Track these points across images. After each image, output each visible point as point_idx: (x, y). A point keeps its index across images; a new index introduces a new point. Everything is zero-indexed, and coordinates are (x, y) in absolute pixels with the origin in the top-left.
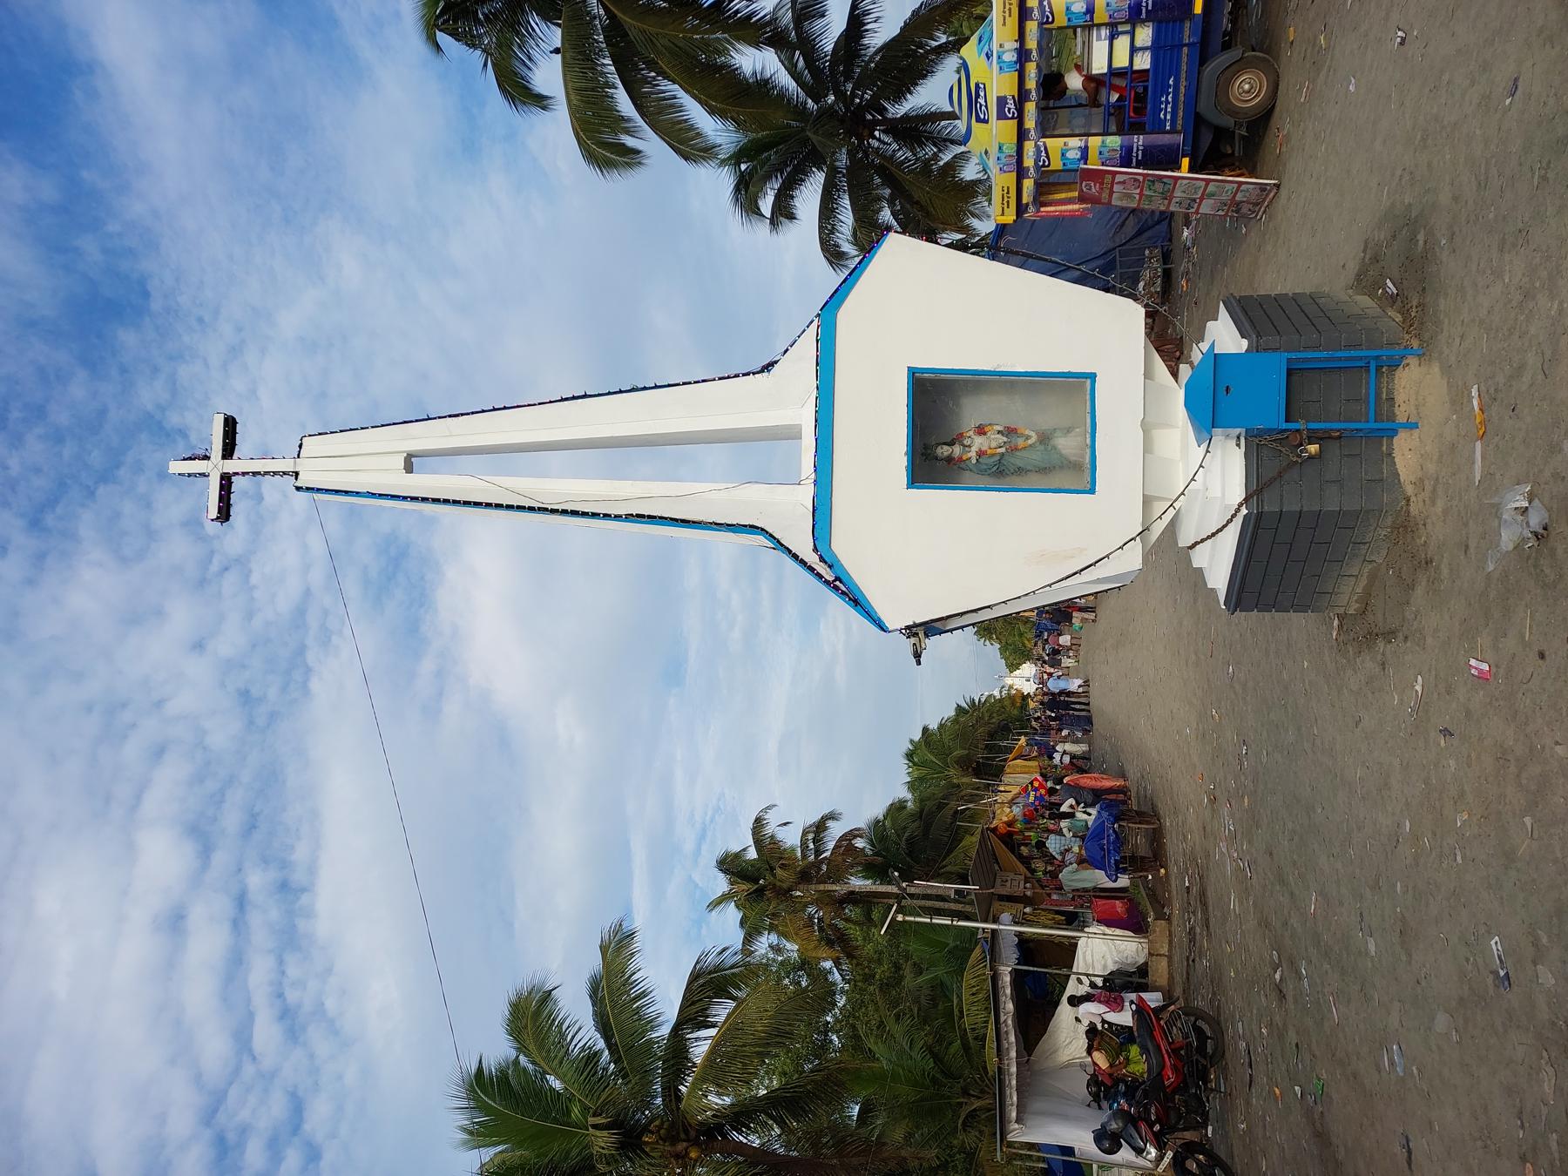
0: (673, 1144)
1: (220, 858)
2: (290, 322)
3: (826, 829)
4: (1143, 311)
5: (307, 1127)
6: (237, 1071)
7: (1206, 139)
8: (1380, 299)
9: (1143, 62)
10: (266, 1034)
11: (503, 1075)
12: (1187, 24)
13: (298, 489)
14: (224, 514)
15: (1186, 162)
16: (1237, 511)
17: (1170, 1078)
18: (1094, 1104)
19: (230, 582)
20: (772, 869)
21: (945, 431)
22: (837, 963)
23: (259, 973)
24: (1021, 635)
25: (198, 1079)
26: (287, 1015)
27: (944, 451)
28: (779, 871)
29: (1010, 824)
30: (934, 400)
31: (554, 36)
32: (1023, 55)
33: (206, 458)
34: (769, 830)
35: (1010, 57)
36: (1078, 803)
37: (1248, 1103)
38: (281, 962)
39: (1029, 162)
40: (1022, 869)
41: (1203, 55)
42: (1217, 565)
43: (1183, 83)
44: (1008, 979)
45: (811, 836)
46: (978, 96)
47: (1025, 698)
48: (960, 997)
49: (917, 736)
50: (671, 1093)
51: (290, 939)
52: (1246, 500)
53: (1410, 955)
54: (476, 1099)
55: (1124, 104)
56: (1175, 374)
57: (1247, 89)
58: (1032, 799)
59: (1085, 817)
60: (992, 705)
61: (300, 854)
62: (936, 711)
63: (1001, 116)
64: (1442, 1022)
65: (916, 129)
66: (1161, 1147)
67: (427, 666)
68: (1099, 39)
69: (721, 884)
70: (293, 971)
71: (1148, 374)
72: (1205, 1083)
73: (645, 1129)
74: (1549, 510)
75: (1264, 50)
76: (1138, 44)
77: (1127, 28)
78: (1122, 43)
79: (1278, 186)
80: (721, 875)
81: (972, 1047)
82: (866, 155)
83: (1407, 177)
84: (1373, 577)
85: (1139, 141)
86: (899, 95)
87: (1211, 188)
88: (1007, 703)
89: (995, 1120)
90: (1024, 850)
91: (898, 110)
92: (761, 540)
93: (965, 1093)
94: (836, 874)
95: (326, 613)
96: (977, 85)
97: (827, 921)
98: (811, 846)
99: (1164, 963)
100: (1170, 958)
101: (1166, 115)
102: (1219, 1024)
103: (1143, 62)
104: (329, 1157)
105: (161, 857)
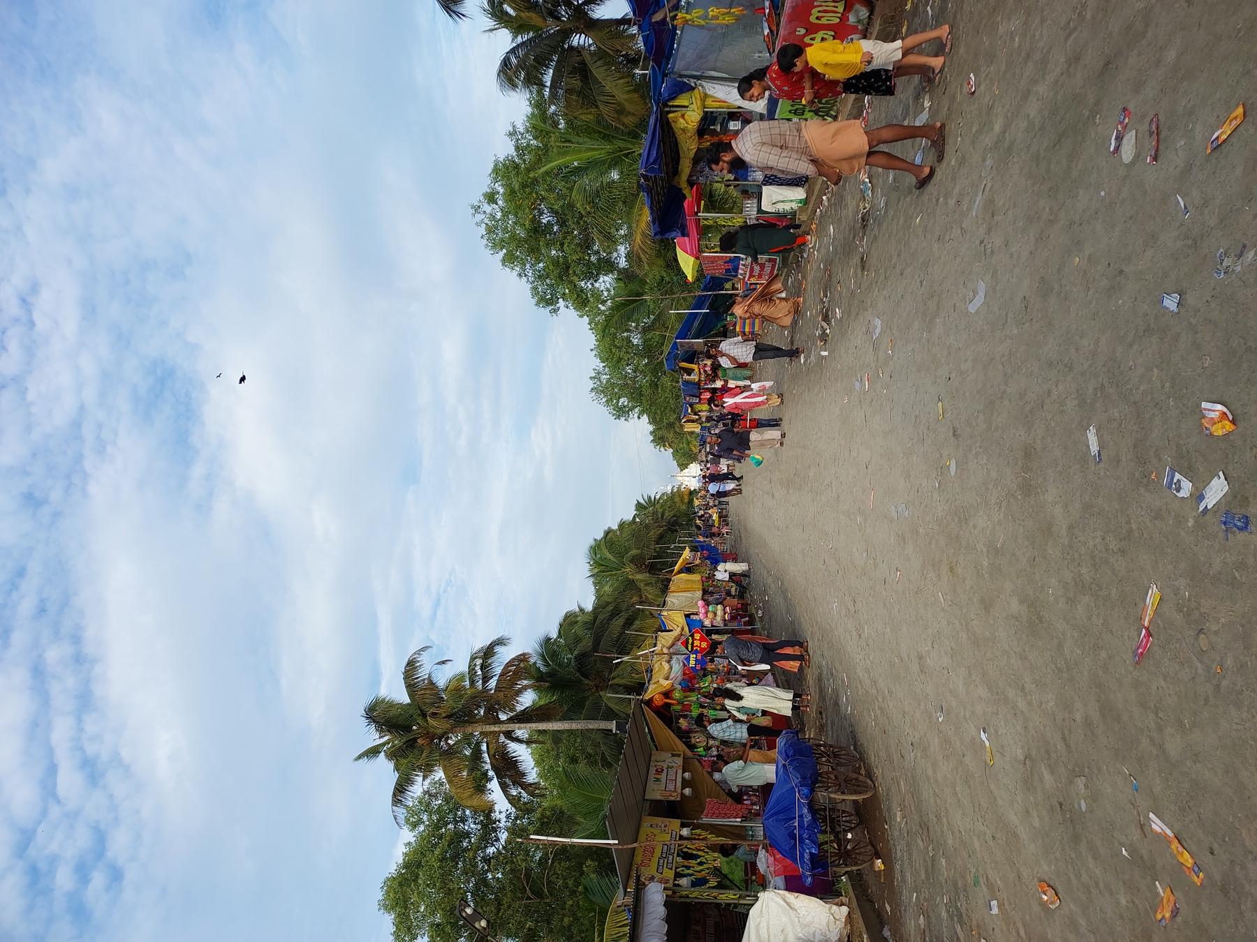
3: (493, 654)
5: (110, 854)
6: (45, 812)
10: (69, 781)
23: (61, 731)
24: (688, 443)
29: (667, 694)
34: (423, 673)
40: (681, 747)
45: (479, 662)
47: (692, 493)
49: (600, 536)
51: (85, 701)
60: (666, 501)
62: (619, 510)
67: (198, 470)
69: (373, 737)
70: (90, 728)
88: (677, 499)
90: (683, 723)
98: (479, 672)
104: (131, 874)
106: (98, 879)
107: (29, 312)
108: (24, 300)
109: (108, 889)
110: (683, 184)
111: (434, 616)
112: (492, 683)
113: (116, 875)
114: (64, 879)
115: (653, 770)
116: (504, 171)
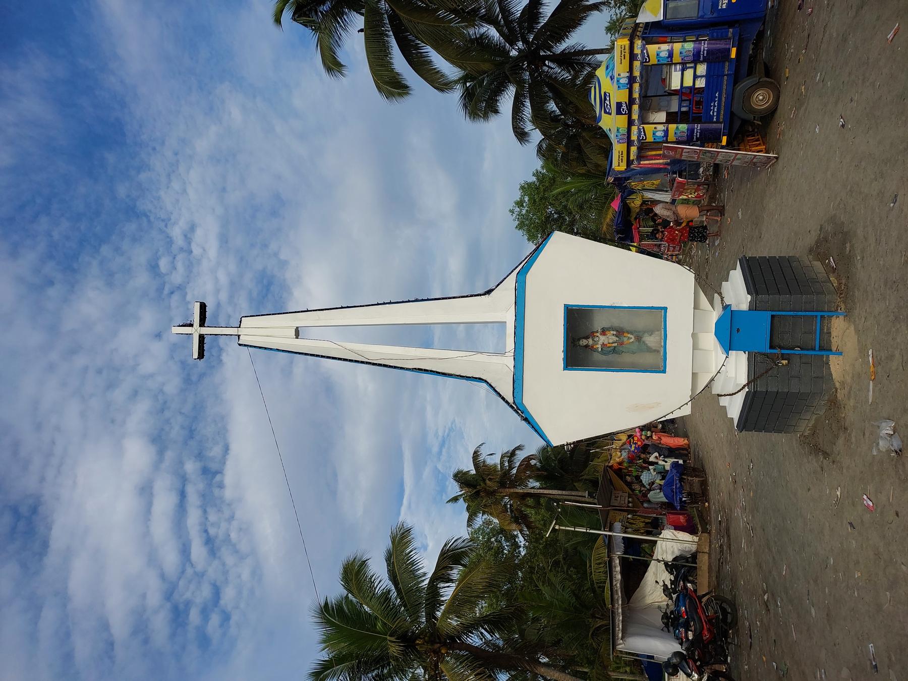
0: (432, 645)
1: (169, 455)
2: (202, 146)
4: (691, 276)
5: (222, 602)
6: (183, 572)
7: (737, 124)
8: (827, 266)
9: (701, 83)
10: (198, 551)
11: (339, 607)
12: (727, 64)
13: (240, 345)
14: (201, 355)
15: (725, 139)
16: (743, 388)
17: (706, 636)
18: (666, 629)
19: (175, 298)
20: (484, 480)
21: (585, 339)
22: (521, 531)
23: (193, 517)
25: (163, 577)
26: (209, 541)
27: (584, 342)
28: (487, 482)
29: (620, 463)
30: (578, 321)
31: (358, 21)
32: (632, 79)
33: (191, 325)
35: (624, 81)
36: (660, 456)
37: (749, 656)
38: (205, 512)
39: (634, 137)
40: (627, 489)
41: (736, 79)
42: (734, 408)
43: (724, 96)
44: (617, 561)
46: (605, 99)
48: (590, 566)
50: (431, 616)
52: (748, 384)
53: (831, 628)
54: (324, 618)
55: (692, 107)
56: (712, 303)
57: (761, 99)
58: (633, 449)
59: (664, 463)
61: (216, 451)
63: (619, 112)
64: (845, 673)
65: (571, 59)
66: (701, 674)
68: (675, 70)
69: (454, 489)
70: (212, 517)
71: (696, 307)
72: (726, 639)
73: (418, 637)
74: (903, 442)
75: (770, 75)
76: (698, 73)
77: (692, 65)
78: (689, 73)
79: (777, 158)
80: (408, 84)
81: (597, 590)
82: (540, 75)
83: (842, 206)
84: (817, 420)
85: (698, 127)
86: (560, 38)
87: (738, 156)
89: (608, 633)
90: (628, 479)
91: (561, 47)
92: (484, 385)
93: (593, 616)
94: (519, 480)
95: (229, 317)
96: (605, 93)
97: (515, 506)
99: (706, 557)
100: (709, 554)
101: (714, 112)
102: (735, 605)
103: (701, 83)
104: (235, 618)
105: (137, 454)
106: (215, 619)
107: (190, 243)
108: (185, 236)
109: (221, 626)
110: (632, 219)
111: (440, 453)
112: (514, 471)
113: (226, 617)
114: (194, 616)
115: (613, 497)
116: (526, 188)
